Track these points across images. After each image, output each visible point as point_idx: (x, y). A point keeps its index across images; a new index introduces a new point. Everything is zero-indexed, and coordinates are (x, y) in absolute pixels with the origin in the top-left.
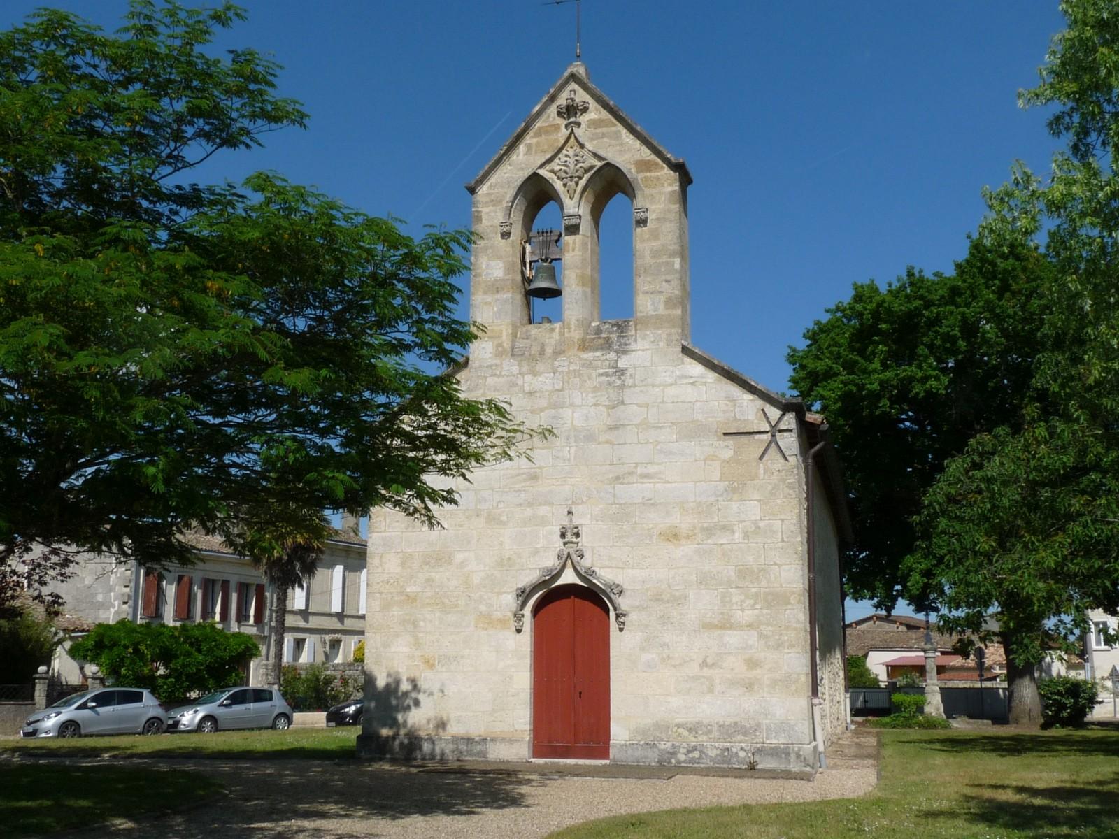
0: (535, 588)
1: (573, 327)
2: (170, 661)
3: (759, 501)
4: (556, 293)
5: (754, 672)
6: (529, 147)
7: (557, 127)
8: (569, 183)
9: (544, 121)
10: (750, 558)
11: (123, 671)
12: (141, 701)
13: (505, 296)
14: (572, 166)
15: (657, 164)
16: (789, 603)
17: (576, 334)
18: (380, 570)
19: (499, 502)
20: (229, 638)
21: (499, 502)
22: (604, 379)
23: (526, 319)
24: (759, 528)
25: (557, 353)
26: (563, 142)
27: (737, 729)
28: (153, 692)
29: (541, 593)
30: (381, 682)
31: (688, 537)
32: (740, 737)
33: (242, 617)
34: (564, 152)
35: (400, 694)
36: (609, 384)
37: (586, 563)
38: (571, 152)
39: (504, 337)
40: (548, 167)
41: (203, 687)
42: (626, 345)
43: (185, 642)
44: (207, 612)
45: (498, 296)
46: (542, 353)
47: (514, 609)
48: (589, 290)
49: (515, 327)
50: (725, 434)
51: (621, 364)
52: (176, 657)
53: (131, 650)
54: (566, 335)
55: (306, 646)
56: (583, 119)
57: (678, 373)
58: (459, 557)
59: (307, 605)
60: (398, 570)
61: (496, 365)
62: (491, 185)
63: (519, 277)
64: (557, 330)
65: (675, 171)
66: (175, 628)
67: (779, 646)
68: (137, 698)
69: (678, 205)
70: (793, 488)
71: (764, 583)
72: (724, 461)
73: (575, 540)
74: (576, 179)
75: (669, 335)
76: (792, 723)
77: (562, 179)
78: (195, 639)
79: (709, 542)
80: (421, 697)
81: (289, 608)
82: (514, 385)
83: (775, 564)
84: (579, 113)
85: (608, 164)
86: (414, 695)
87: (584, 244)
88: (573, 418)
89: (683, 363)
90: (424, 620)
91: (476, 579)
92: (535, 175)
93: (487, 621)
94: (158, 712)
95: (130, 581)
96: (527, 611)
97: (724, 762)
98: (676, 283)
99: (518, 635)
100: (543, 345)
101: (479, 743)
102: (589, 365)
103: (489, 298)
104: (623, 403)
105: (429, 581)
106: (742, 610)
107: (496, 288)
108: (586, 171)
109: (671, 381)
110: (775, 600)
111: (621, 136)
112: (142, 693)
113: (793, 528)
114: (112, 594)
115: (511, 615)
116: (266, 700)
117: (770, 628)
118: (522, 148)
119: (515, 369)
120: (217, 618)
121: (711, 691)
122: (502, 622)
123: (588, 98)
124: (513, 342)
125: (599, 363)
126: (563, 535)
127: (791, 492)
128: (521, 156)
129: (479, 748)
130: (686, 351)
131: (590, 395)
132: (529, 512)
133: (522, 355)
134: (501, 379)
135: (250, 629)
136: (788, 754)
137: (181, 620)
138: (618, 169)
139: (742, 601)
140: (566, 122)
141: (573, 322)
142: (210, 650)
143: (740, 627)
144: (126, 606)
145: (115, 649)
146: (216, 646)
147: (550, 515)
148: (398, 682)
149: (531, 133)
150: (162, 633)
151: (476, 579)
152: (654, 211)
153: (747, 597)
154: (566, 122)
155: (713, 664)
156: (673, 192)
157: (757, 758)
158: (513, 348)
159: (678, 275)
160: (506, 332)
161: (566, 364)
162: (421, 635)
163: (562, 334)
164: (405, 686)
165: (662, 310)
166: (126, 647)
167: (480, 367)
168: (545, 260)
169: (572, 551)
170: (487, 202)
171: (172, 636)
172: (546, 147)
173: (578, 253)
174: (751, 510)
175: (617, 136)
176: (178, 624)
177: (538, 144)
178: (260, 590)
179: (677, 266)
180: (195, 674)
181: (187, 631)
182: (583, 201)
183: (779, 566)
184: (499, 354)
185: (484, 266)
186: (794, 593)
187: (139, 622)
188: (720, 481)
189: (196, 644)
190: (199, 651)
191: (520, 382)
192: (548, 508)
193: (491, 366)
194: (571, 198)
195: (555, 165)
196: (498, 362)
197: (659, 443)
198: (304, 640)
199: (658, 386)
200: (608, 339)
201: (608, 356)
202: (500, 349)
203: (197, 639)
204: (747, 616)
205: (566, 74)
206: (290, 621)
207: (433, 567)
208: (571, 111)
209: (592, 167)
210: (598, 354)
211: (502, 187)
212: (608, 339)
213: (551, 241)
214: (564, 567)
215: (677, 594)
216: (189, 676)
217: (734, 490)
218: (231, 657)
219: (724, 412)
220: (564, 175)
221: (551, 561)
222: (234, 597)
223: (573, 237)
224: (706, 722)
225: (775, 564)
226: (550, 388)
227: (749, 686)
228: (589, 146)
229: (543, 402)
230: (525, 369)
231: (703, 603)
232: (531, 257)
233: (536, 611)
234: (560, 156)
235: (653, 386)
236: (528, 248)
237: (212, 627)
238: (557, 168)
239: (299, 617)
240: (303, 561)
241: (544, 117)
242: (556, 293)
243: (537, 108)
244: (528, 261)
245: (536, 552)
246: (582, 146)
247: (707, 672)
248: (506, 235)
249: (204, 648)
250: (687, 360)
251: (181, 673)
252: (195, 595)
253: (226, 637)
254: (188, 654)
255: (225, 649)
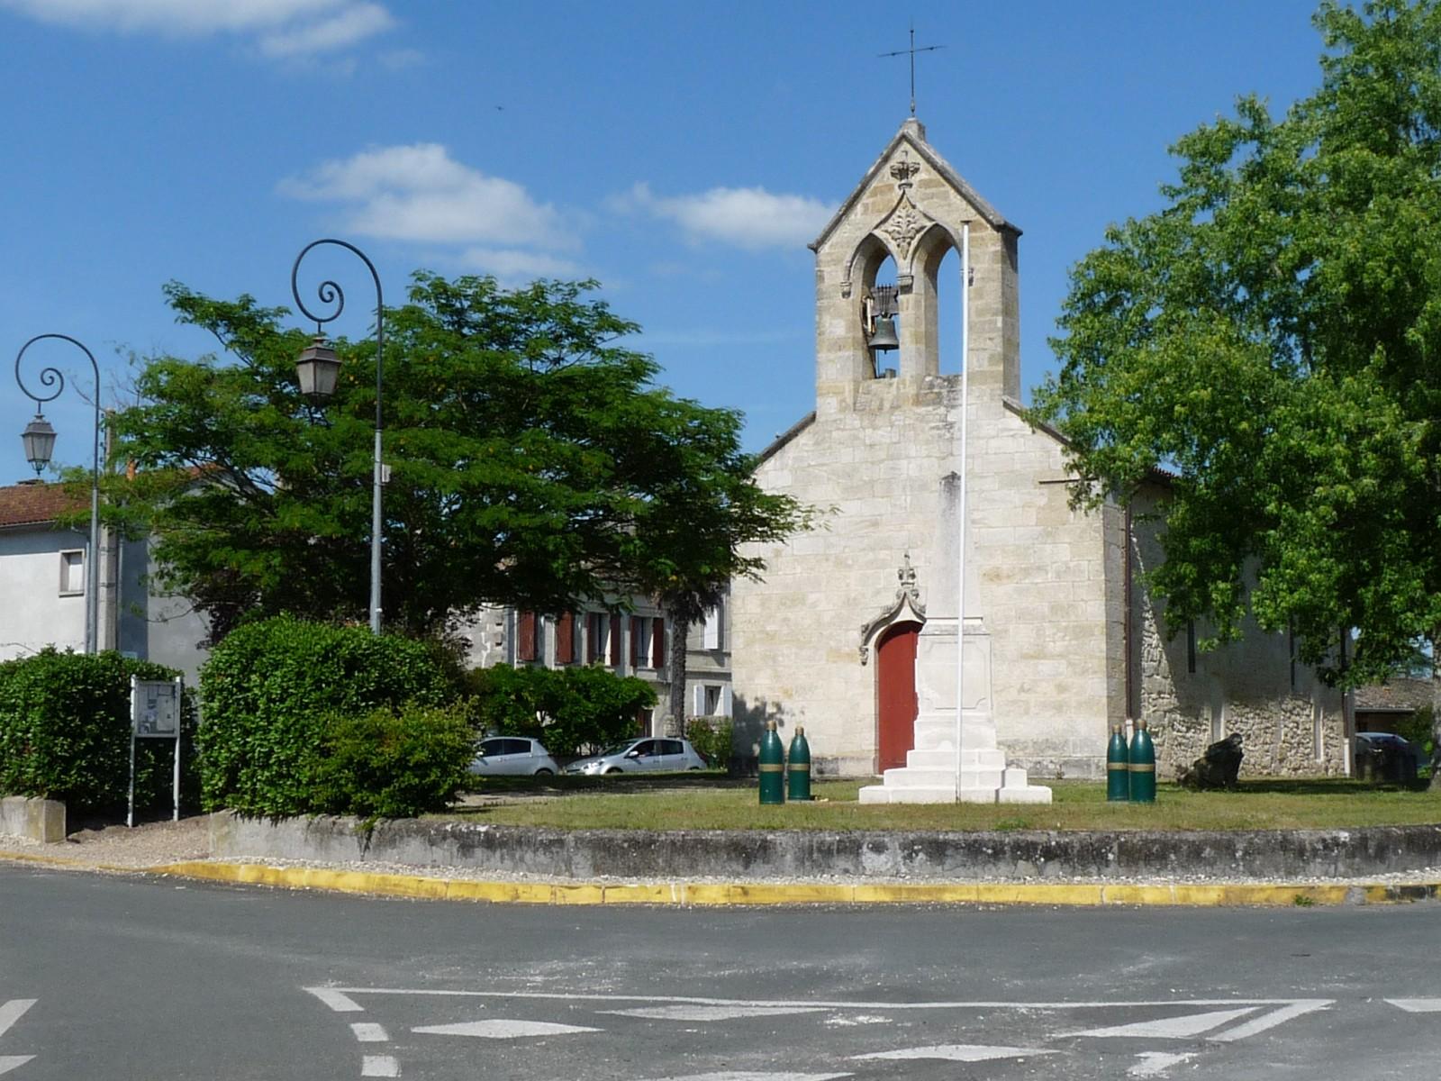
0: (877, 625)
1: (908, 383)
2: (557, 709)
3: (1070, 543)
4: (896, 347)
5: (1063, 696)
6: (866, 206)
7: (891, 187)
8: (902, 244)
9: (880, 181)
10: (1061, 596)
11: (506, 721)
12: (529, 750)
13: (847, 354)
14: (904, 226)
15: (981, 224)
16: (1093, 635)
17: (911, 390)
18: (742, 611)
19: (845, 547)
20: (621, 683)
21: (845, 547)
22: (935, 432)
23: (870, 372)
24: (1069, 568)
25: (894, 408)
26: (896, 202)
27: (1050, 745)
28: (540, 742)
29: (882, 629)
30: (750, 705)
31: (1008, 577)
32: (1051, 752)
33: (637, 660)
34: (897, 213)
35: (767, 715)
36: (940, 436)
37: (921, 601)
38: (903, 214)
39: (847, 394)
40: (883, 227)
41: (595, 740)
42: (954, 399)
43: (571, 688)
44: (596, 653)
45: (840, 354)
46: (881, 408)
47: (860, 644)
48: (923, 347)
49: (856, 383)
50: (1041, 483)
51: (950, 419)
52: (562, 705)
53: (513, 697)
54: (902, 391)
55: (722, 695)
56: (914, 179)
57: (1000, 426)
58: (812, 597)
59: (721, 643)
60: (759, 610)
61: (841, 420)
62: (831, 245)
63: (861, 334)
64: (895, 385)
65: (998, 231)
66: (559, 672)
67: (1084, 672)
68: (525, 747)
69: (1000, 265)
70: (1099, 532)
71: (1073, 618)
72: (1039, 508)
73: (911, 581)
74: (908, 240)
75: (992, 390)
76: (1094, 739)
77: (896, 240)
78: (587, 685)
79: (1027, 581)
80: (785, 718)
81: (690, 647)
82: (857, 438)
83: (1082, 600)
84: (910, 173)
85: (937, 225)
86: (778, 716)
87: (917, 302)
88: (908, 469)
89: (1004, 417)
90: (783, 655)
91: (826, 618)
92: (871, 235)
93: (836, 655)
94: (549, 763)
95: (503, 619)
96: (871, 645)
97: (1037, 774)
98: (999, 340)
99: (864, 667)
100: (882, 400)
101: (832, 761)
102: (922, 419)
103: (832, 356)
104: (952, 454)
105: (786, 620)
106: (1054, 642)
107: (838, 346)
108: (918, 231)
109: (993, 433)
110: (1081, 632)
111: (948, 197)
112: (530, 743)
113: (1098, 568)
114: (483, 634)
115: (857, 650)
116: (676, 753)
117: (1077, 657)
118: (859, 208)
119: (857, 423)
120: (608, 661)
121: (1027, 713)
122: (850, 656)
123: (919, 159)
124: (855, 398)
125: (931, 417)
126: (901, 577)
127: (1097, 535)
128: (859, 216)
129: (831, 766)
130: (1007, 405)
131: (924, 447)
132: (871, 556)
133: (864, 410)
134: (845, 433)
135: (648, 674)
136: (1089, 765)
137: (564, 664)
138: (946, 230)
139: (1055, 634)
140: (899, 183)
141: (908, 378)
142: (600, 697)
143: (1052, 657)
144: (500, 648)
145: (497, 696)
146: (606, 691)
147: (889, 558)
148: (765, 704)
149: (868, 192)
150: (545, 678)
151: (826, 618)
152: (979, 271)
153: (1058, 631)
154: (899, 183)
155: (1029, 689)
156: (997, 252)
157: (1063, 770)
158: (855, 404)
159: (1001, 333)
160: (848, 388)
161: (902, 418)
162: (780, 669)
163: (898, 388)
164: (770, 709)
165: (986, 367)
166: (508, 694)
167: (827, 421)
168: (885, 316)
169: (908, 591)
170: (828, 262)
171: (558, 682)
172: (881, 207)
173: (911, 311)
174: (1062, 552)
175: (945, 196)
176: (562, 668)
177: (874, 203)
178: (659, 626)
179: (1000, 324)
180: (586, 724)
181: (573, 675)
182: (915, 260)
183: (1086, 602)
184: (842, 410)
185: (827, 325)
186: (1097, 625)
187: (516, 667)
188: (1036, 525)
189: (584, 690)
190: (588, 698)
191: (861, 435)
192: (887, 552)
193: (835, 421)
194: (905, 258)
195: (889, 226)
196: (842, 416)
197: (983, 491)
198: (720, 688)
199: (983, 438)
200: (940, 393)
201: (938, 411)
202: (844, 404)
203: (585, 684)
204: (1058, 647)
205: (898, 136)
206: (692, 663)
207: (790, 607)
208: (903, 172)
209: (923, 228)
210: (930, 408)
211: (842, 247)
212: (940, 393)
213: (888, 298)
214: (901, 606)
215: (999, 628)
216: (579, 727)
217: (1049, 534)
218: (625, 705)
219: (1041, 462)
220: (897, 236)
221: (891, 601)
222: (627, 636)
223: (907, 296)
224: (1023, 739)
225: (1082, 600)
226: (888, 441)
227: (1059, 708)
228: (919, 206)
229: (883, 455)
230: (866, 423)
231: (1021, 636)
232: (872, 312)
233: (880, 645)
234: (894, 216)
235: (979, 438)
236: (870, 303)
237: (600, 670)
238: (890, 229)
239: (711, 659)
240: (703, 592)
241: (879, 176)
242: (896, 347)
243: (872, 170)
244: (869, 316)
245: (878, 592)
246: (914, 207)
247: (1024, 696)
248: (846, 294)
249: (593, 694)
250: (1008, 413)
251: (570, 723)
252: (580, 632)
253: (617, 682)
254: (576, 702)
255: (617, 696)
